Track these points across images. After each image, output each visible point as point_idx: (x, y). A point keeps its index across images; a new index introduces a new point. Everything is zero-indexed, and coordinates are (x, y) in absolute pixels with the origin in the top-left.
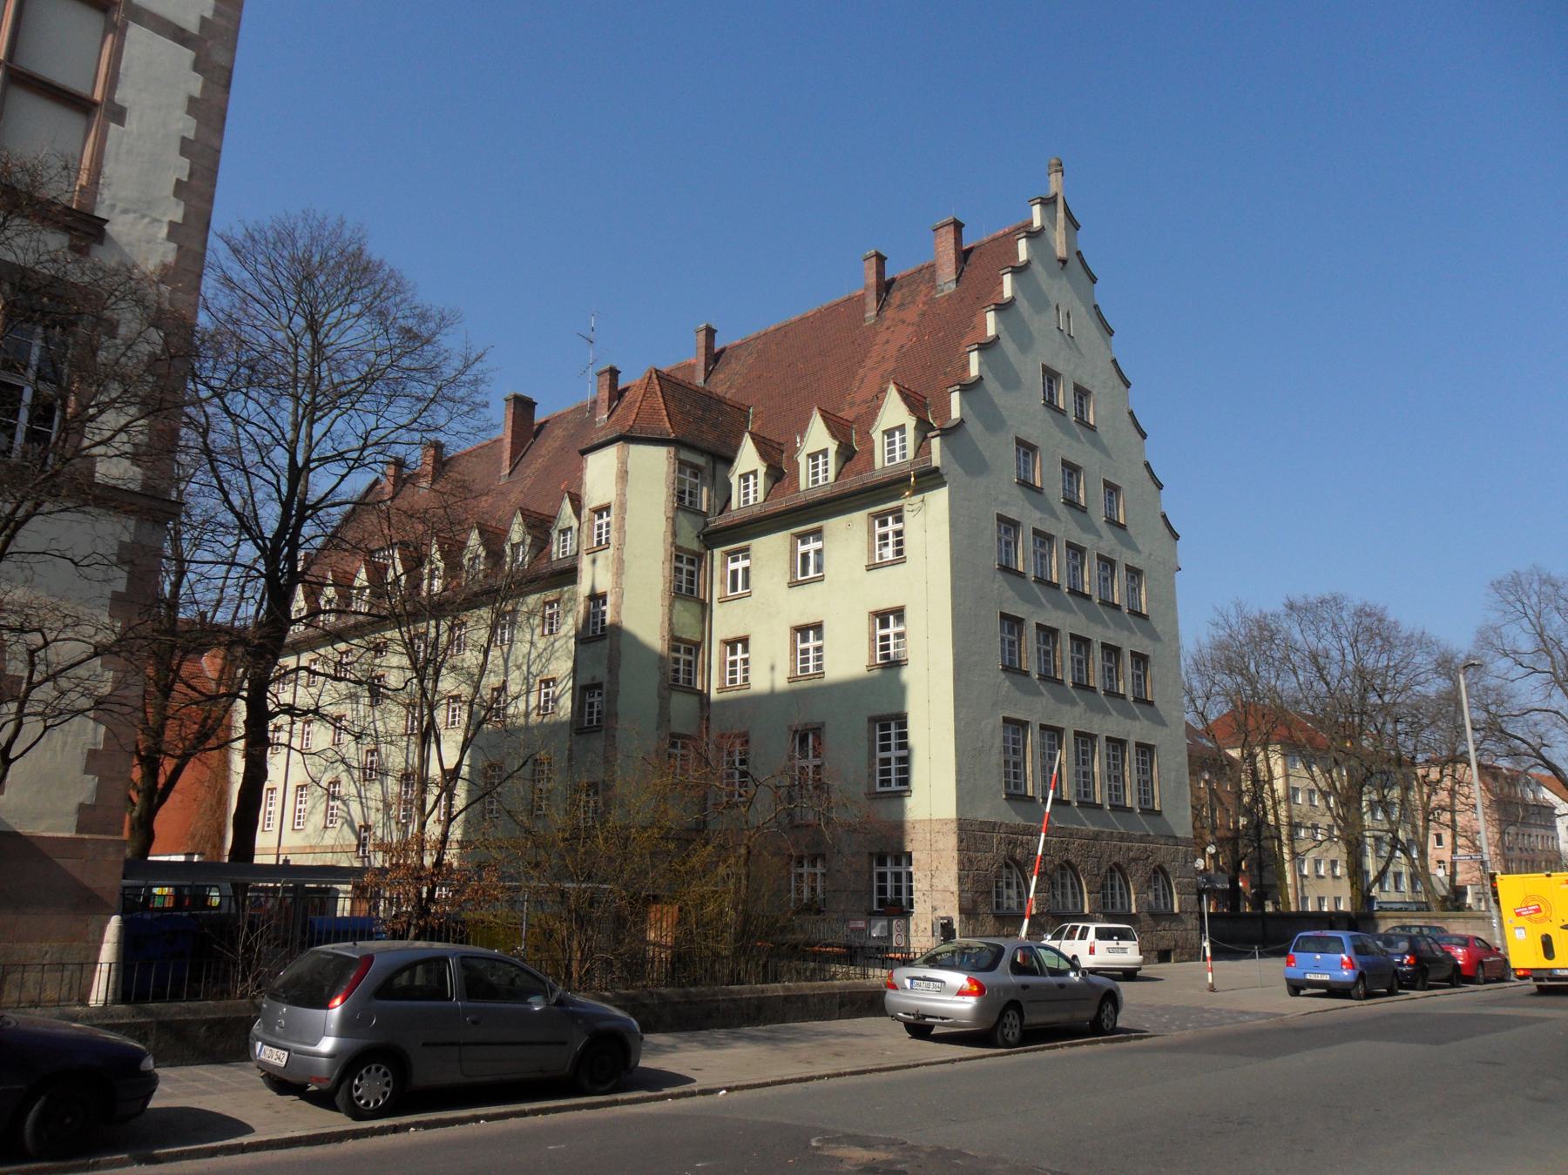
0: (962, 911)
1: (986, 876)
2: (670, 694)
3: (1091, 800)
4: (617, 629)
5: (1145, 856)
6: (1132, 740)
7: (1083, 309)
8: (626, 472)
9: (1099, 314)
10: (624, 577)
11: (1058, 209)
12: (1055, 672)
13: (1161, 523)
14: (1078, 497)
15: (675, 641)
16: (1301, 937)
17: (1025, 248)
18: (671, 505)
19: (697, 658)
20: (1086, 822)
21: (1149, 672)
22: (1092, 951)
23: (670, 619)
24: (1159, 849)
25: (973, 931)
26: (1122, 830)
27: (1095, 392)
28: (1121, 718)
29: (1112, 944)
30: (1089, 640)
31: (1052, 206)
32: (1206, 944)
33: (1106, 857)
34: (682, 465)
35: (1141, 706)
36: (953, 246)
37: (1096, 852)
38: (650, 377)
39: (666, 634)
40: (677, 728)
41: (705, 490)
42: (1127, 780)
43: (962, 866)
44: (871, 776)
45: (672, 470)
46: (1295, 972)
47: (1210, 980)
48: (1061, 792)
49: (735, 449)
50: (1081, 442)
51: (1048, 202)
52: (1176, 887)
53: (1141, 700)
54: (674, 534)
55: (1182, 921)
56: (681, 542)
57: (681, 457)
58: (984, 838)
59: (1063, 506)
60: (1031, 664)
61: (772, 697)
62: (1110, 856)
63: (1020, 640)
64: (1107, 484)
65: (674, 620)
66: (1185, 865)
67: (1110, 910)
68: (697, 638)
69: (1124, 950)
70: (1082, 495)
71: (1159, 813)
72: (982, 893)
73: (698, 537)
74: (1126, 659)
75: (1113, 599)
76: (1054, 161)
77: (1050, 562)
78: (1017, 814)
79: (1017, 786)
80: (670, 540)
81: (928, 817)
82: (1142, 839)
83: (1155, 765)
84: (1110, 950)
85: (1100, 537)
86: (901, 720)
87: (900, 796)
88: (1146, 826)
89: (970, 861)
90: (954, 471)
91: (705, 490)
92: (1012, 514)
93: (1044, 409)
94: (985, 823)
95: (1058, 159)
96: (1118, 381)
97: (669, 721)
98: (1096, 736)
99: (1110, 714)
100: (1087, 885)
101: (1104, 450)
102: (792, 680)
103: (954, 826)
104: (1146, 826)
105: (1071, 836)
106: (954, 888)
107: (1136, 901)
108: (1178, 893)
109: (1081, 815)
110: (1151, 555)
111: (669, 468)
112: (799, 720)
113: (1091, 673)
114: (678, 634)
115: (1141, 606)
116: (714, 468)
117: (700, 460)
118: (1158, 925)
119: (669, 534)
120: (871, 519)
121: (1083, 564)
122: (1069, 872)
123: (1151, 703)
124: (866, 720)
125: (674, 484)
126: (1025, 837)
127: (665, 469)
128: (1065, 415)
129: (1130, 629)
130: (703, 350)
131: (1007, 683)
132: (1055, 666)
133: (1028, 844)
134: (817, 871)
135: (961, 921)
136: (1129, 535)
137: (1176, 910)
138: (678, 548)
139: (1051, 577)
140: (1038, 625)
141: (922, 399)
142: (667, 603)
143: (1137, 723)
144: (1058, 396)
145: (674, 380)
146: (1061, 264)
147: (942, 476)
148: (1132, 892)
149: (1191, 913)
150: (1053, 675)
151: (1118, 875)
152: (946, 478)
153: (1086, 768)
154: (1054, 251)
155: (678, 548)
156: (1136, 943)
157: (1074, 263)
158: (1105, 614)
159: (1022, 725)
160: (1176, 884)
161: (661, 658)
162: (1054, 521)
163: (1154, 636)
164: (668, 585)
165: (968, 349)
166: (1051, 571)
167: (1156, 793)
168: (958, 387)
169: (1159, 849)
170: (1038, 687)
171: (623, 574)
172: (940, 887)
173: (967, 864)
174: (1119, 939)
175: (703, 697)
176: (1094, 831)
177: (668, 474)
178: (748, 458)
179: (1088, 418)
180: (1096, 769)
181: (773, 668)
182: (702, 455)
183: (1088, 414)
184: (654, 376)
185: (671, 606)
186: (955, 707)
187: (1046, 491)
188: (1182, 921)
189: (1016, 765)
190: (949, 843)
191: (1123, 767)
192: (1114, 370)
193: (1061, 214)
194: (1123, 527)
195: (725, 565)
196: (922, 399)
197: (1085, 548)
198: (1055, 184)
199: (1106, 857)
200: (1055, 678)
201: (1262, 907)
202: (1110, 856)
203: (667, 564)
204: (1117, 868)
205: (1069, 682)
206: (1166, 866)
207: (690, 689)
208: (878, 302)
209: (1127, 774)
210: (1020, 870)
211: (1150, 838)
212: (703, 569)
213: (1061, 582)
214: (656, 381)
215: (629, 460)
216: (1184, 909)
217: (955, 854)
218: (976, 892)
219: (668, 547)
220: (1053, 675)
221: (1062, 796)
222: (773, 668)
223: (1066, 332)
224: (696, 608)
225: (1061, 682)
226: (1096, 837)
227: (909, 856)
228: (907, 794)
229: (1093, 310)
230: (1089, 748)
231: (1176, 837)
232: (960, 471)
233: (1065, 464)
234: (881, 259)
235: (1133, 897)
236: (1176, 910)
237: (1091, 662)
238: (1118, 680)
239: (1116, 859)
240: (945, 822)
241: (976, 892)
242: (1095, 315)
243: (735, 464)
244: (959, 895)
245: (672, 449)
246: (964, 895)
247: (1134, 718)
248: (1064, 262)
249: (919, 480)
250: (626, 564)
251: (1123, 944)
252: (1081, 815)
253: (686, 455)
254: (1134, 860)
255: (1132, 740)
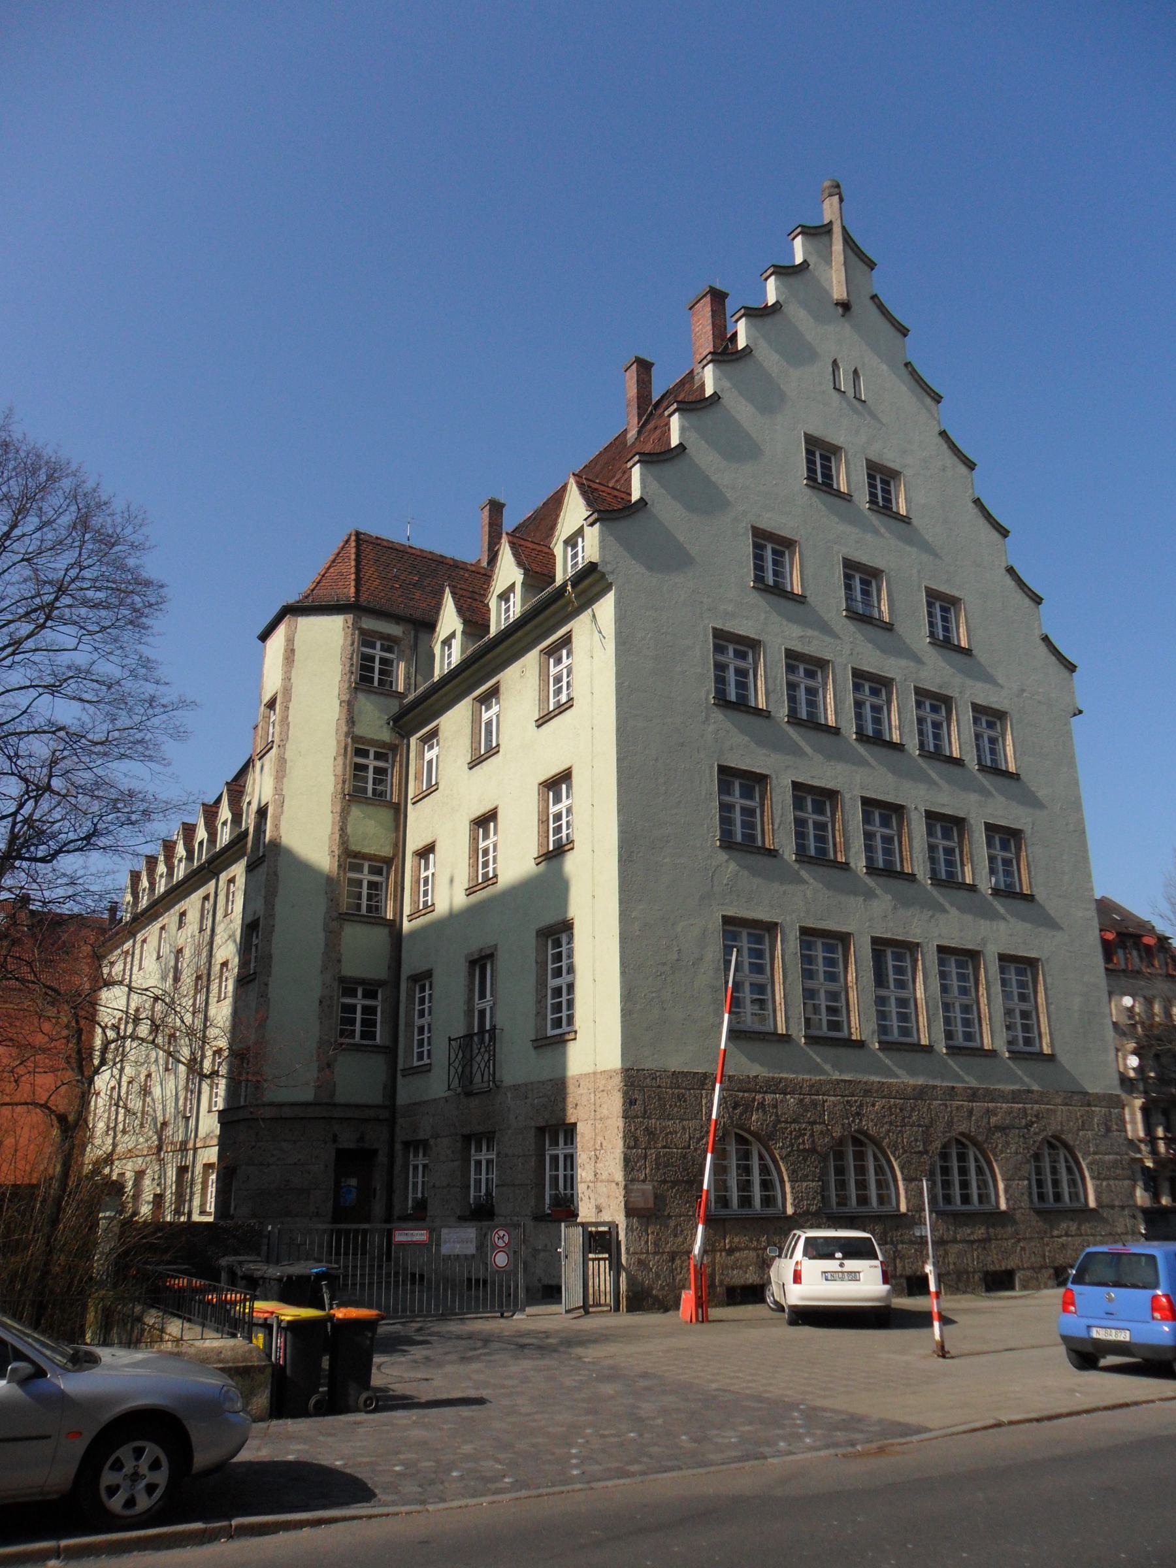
0: (630, 1212)
1: (684, 1156)
2: (341, 927)
3: (914, 1040)
4: (276, 846)
5: (1024, 1122)
6: (991, 952)
7: (884, 367)
8: (293, 651)
9: (914, 373)
10: (285, 780)
11: (834, 240)
12: (902, 865)
13: (1043, 649)
14: (880, 611)
15: (350, 857)
16: (1088, 1254)
17: (774, 288)
18: (346, 685)
19: (388, 878)
20: (899, 1072)
21: (1023, 854)
22: (797, 1278)
23: (343, 830)
24: (1055, 1111)
25: (656, 1244)
26: (974, 1083)
27: (908, 472)
28: (968, 918)
29: (831, 1265)
30: (902, 807)
31: (825, 239)
32: (929, 1268)
33: (940, 1126)
34: (366, 638)
35: (1008, 901)
36: (710, 321)
37: (920, 1118)
38: (347, 541)
39: (335, 848)
40: (350, 969)
41: (402, 665)
42: (984, 1009)
43: (631, 1140)
44: (540, 1014)
45: (349, 642)
46: (1073, 1324)
47: (937, 1337)
48: (849, 1028)
49: (438, 607)
50: (882, 536)
51: (817, 233)
52: (1091, 1170)
53: (1007, 893)
54: (351, 721)
55: (1104, 1220)
56: (360, 730)
57: (364, 626)
58: (681, 1097)
59: (846, 621)
60: (916, 861)
61: (453, 918)
62: (950, 1123)
63: (762, 805)
64: (933, 596)
65: (349, 830)
66: (1105, 1136)
67: (958, 1204)
68: (386, 851)
69: (854, 1276)
70: (884, 607)
71: (1051, 1058)
72: (675, 1183)
73: (389, 724)
74: (976, 835)
75: (951, 751)
76: (827, 183)
77: (825, 698)
78: (752, 1060)
79: (1028, 1041)
80: (345, 729)
81: (590, 1069)
82: (1015, 1097)
83: (1041, 988)
84: (827, 1276)
85: (919, 661)
86: (567, 927)
87: (561, 1041)
88: (1025, 1078)
89: (649, 1132)
90: (627, 569)
91: (402, 665)
92: (744, 628)
93: (808, 491)
94: (685, 1074)
95: (833, 180)
96: (950, 460)
97: (339, 961)
98: (918, 945)
99: (944, 911)
100: (902, 1169)
101: (926, 547)
102: (470, 892)
103: (617, 1081)
104: (1025, 1078)
105: (867, 1092)
106: (619, 1176)
107: (1006, 1191)
108: (1093, 1178)
109: (887, 1061)
110: (1023, 691)
111: (345, 639)
112: (474, 945)
113: (906, 854)
114: (354, 847)
115: (1006, 762)
116: (416, 638)
117: (395, 630)
118: (1052, 1228)
119: (343, 723)
120: (544, 657)
121: (889, 702)
122: (1062, 1152)
123: (1030, 898)
124: (534, 934)
125: (351, 659)
126: (769, 1097)
127: (341, 642)
128: (909, 523)
129: (983, 791)
130: (487, 529)
131: (732, 866)
132: (835, 845)
133: (775, 1106)
134: (559, 1152)
135: (629, 1229)
136: (979, 663)
137: (1092, 1203)
138: (356, 739)
139: (826, 719)
140: (796, 786)
141: (623, 496)
142: (338, 809)
143: (1002, 926)
144: (838, 477)
145: (385, 544)
146: (840, 310)
147: (603, 576)
148: (999, 1177)
149: (1123, 1208)
150: (832, 857)
151: (971, 1153)
152: (610, 578)
153: (904, 994)
154: (828, 294)
155: (356, 739)
156: (877, 1263)
157: (864, 307)
158: (932, 770)
159: (971, 957)
160: (1089, 1165)
161: (329, 880)
162: (828, 639)
163: (1032, 801)
164: (340, 786)
165: (666, 413)
166: (826, 710)
167: (1044, 1028)
168: (637, 458)
169: (1055, 1111)
170: (797, 873)
171: (284, 777)
172: (605, 1176)
173: (643, 1140)
174: (844, 1258)
175: (394, 926)
176: (914, 1088)
177: (343, 648)
178: (450, 620)
179: (898, 507)
180: (920, 993)
181: (452, 881)
182: (398, 624)
183: (897, 503)
184: (353, 538)
185: (344, 815)
186: (621, 902)
187: (811, 599)
188: (1104, 1220)
189: (1025, 1015)
190: (614, 1104)
191: (977, 991)
192: (945, 446)
193: (838, 246)
194: (967, 652)
195: (421, 755)
196: (623, 496)
197: (892, 679)
198: (830, 211)
199: (940, 1126)
200: (835, 861)
201: (1159, 1202)
202: (950, 1123)
203: (340, 760)
204: (962, 1143)
205: (859, 864)
206: (1068, 1138)
207: (374, 916)
208: (640, 416)
209: (983, 1001)
210: (979, 1150)
211: (1035, 1096)
212: (397, 764)
213: (966, 758)
214: (353, 544)
215: (296, 638)
216: (1106, 1200)
217: (620, 1123)
218: (665, 1182)
219: (343, 738)
220: (832, 857)
221: (851, 1034)
222: (452, 881)
223: (851, 393)
224: (386, 815)
225: (845, 866)
226: (921, 1093)
227: (570, 1131)
228: (572, 1036)
229: (903, 370)
230: (971, 971)
231: (1087, 1093)
232: (640, 569)
233: (850, 566)
234: (644, 367)
235: (1001, 1186)
236: (1092, 1203)
237: (905, 839)
238: (963, 865)
239: (963, 1128)
240: (608, 1075)
241: (665, 1182)
242: (907, 377)
243: (438, 629)
244: (626, 1187)
245: (350, 617)
246: (637, 1186)
247: (994, 916)
248: (845, 306)
249: (581, 587)
250: (289, 764)
251: (852, 1265)
252: (887, 1061)
253: (369, 623)
254: (998, 1128)
255: (991, 952)
